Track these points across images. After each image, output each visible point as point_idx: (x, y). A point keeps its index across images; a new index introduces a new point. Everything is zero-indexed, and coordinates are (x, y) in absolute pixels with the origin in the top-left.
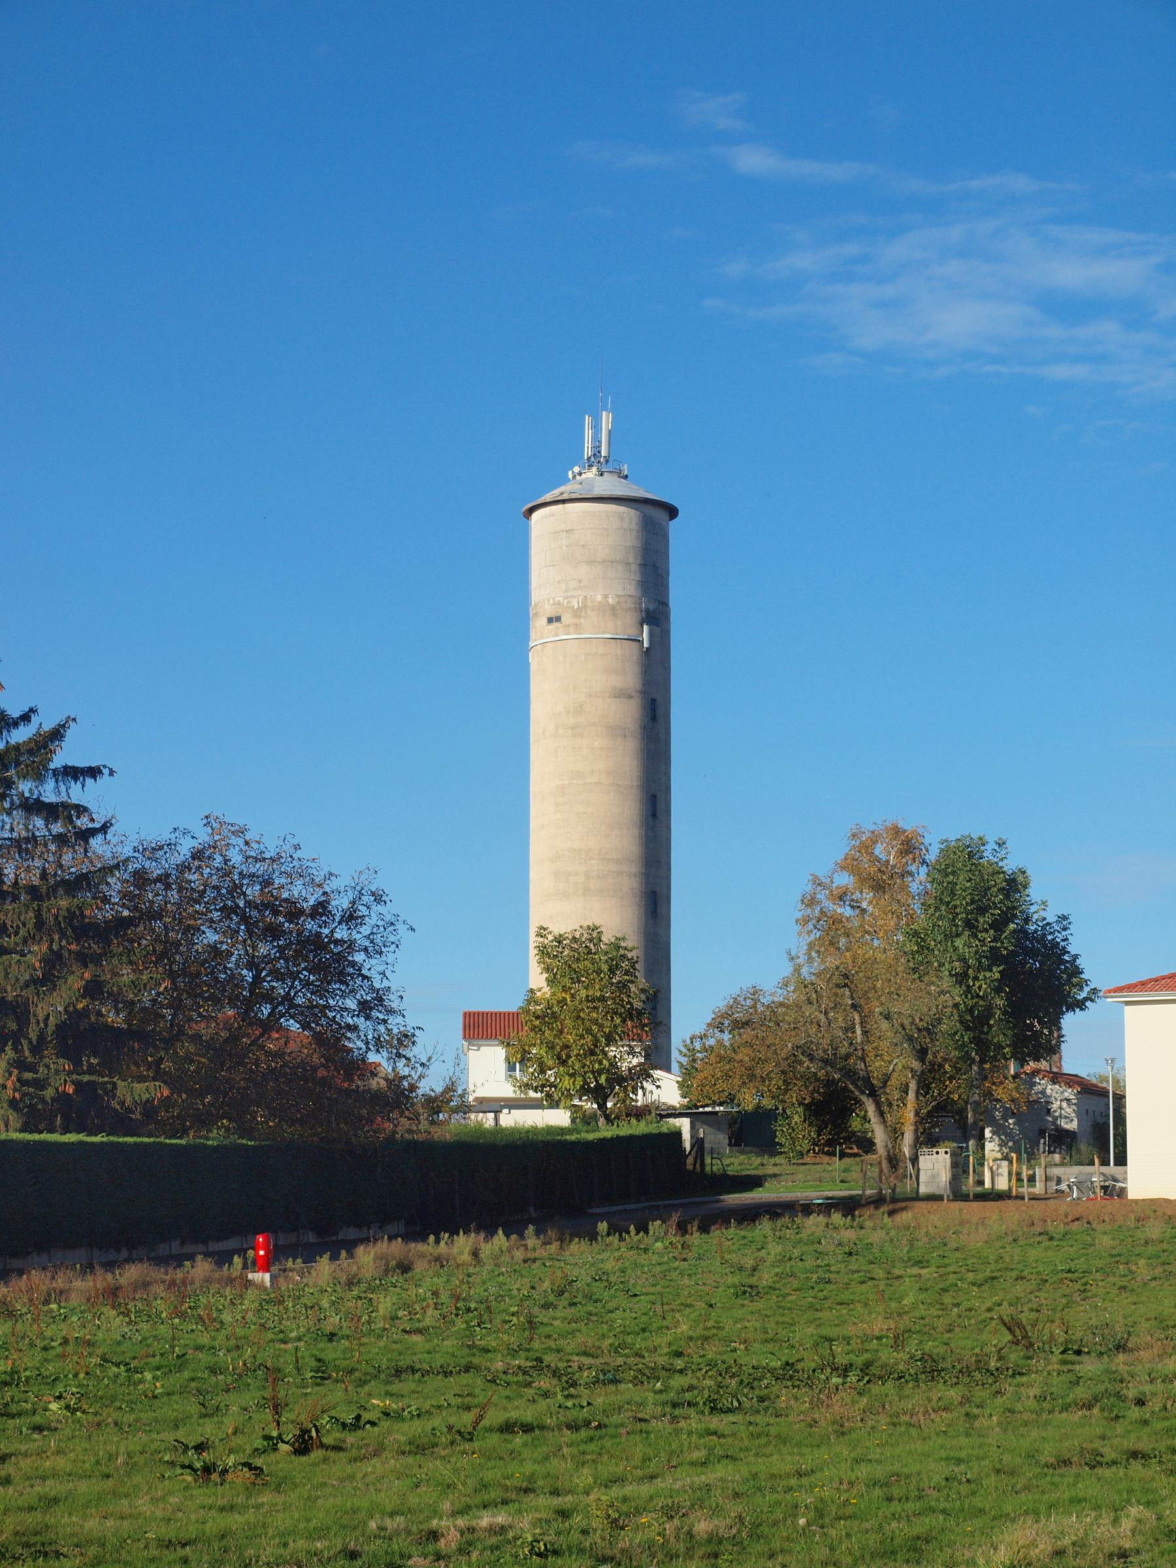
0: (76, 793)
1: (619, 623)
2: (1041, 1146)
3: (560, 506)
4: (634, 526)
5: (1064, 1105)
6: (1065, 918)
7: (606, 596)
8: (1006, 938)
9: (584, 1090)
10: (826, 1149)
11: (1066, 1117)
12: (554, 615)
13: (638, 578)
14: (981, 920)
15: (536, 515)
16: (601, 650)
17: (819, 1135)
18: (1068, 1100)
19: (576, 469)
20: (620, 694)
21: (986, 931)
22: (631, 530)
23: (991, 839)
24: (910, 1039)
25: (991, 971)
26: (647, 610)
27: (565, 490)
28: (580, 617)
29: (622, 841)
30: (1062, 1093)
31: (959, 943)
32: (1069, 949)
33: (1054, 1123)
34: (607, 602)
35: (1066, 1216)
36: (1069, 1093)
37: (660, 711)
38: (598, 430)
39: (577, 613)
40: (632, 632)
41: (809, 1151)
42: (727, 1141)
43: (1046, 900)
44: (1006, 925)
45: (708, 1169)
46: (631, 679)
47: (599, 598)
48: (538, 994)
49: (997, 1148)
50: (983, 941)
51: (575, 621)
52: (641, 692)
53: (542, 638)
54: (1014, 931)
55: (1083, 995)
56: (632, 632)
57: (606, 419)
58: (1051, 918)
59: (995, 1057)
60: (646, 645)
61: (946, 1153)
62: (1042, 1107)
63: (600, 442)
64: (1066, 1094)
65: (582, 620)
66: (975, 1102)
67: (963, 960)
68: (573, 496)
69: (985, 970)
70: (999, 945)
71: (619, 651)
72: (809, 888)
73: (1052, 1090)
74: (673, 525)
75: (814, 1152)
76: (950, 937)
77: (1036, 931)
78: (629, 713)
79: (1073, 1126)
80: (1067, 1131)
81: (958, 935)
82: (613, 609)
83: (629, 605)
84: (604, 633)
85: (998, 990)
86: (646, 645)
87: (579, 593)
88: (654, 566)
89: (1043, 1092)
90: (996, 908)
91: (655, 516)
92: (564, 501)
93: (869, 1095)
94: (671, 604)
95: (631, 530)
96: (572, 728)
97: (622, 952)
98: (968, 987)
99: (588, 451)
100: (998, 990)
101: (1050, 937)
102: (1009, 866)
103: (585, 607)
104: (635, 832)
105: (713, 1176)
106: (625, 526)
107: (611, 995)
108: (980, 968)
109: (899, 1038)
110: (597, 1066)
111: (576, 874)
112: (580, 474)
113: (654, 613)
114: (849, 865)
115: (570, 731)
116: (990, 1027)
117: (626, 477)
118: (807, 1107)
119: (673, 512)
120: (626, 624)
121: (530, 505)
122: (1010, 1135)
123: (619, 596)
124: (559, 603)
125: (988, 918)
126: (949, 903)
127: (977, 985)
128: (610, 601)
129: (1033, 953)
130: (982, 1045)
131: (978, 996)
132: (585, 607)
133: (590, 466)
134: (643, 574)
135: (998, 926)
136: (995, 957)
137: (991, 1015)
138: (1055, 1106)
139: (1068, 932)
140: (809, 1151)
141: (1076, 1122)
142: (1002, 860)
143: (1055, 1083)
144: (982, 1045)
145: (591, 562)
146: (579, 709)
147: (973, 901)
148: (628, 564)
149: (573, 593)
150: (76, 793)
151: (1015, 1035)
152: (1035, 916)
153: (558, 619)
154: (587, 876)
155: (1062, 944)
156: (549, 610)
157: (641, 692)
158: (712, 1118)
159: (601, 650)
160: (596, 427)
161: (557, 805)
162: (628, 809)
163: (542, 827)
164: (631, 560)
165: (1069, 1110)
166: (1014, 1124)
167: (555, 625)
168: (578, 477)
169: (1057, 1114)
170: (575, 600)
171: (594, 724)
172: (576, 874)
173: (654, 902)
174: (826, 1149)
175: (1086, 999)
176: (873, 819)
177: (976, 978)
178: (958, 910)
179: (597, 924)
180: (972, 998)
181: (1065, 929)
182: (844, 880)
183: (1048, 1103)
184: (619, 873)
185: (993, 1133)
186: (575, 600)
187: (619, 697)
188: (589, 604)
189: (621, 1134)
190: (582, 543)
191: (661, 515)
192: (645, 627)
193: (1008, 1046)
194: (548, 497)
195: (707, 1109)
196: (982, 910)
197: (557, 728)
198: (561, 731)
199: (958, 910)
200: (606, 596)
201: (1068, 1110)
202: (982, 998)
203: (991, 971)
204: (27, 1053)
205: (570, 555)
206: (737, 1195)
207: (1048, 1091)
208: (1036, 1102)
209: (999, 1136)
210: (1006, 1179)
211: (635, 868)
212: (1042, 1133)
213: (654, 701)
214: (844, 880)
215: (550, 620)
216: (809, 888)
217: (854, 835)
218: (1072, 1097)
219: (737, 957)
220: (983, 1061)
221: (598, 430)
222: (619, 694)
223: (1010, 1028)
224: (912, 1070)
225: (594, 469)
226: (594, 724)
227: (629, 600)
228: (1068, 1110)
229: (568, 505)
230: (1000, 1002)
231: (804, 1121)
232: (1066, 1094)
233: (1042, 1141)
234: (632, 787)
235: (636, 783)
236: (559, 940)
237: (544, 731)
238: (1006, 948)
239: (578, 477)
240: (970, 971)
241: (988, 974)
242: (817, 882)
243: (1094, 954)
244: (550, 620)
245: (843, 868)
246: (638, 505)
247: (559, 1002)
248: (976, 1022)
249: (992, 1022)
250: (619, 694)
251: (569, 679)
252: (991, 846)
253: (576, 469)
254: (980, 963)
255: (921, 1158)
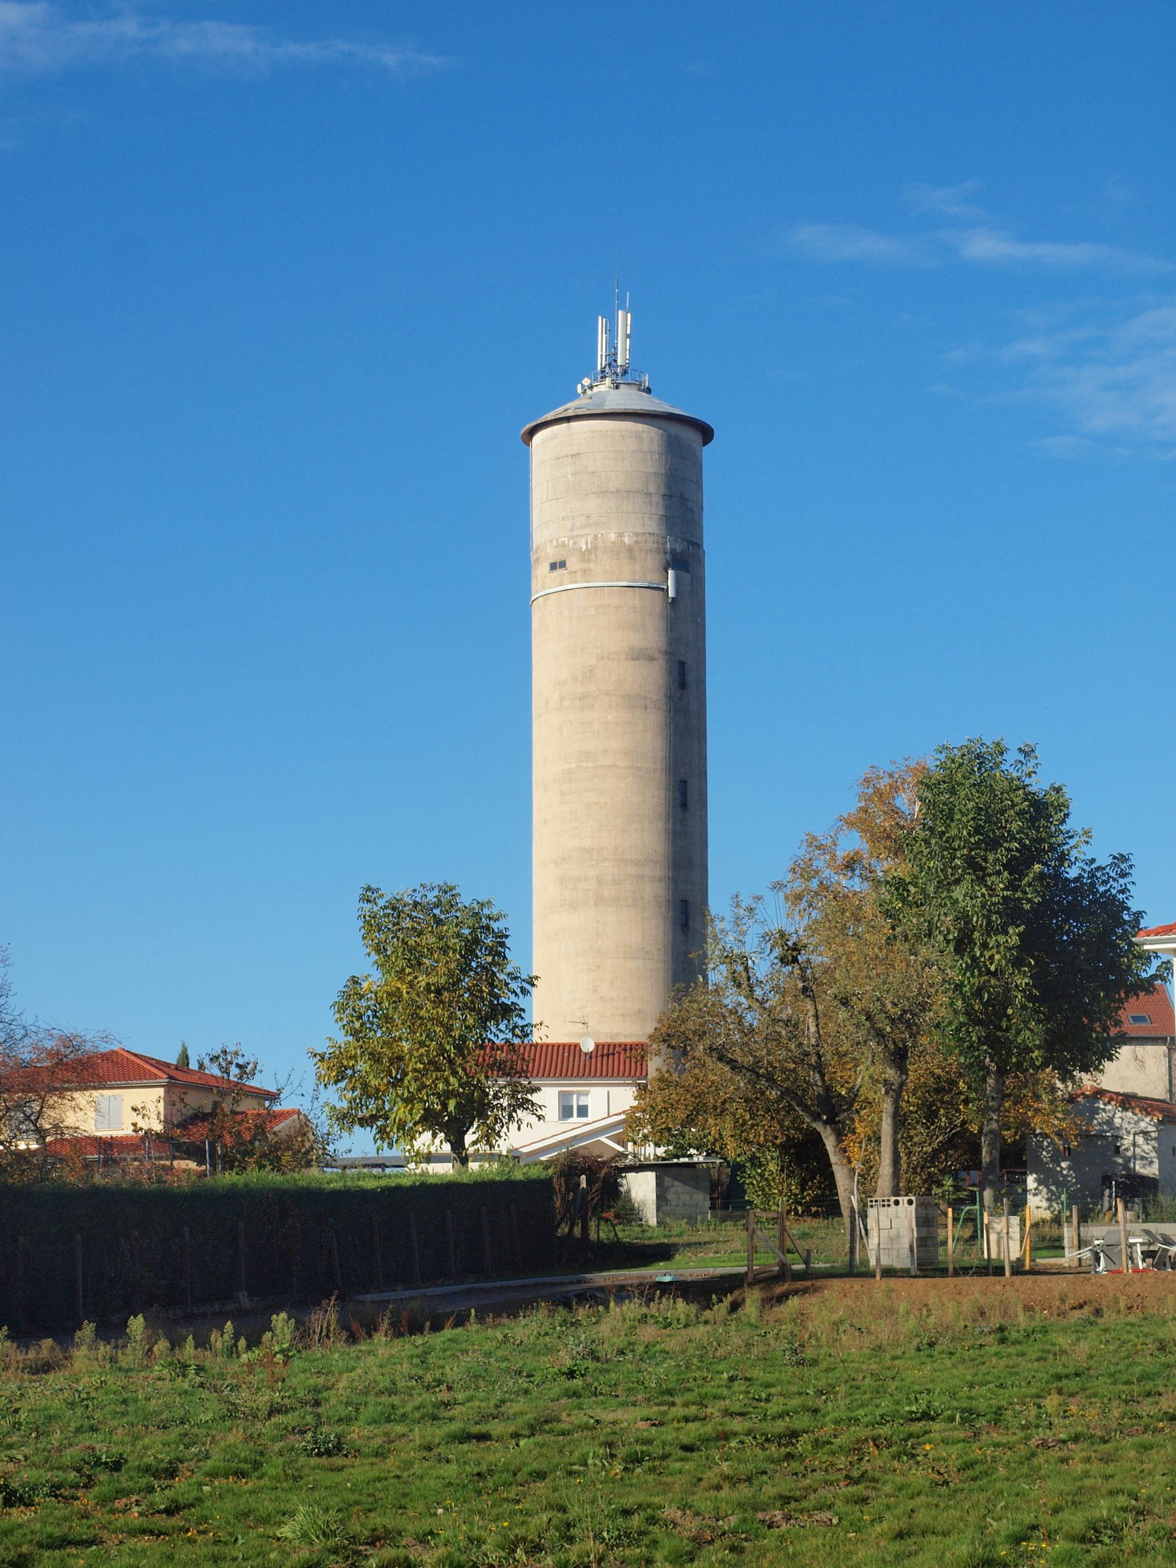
1: (638, 567)
2: (1106, 1199)
3: (565, 426)
4: (655, 447)
5: (1140, 1140)
6: (1123, 858)
7: (621, 535)
8: (1030, 885)
9: (430, 1120)
10: (814, 1209)
11: (1143, 1158)
12: (558, 559)
13: (661, 512)
14: (991, 857)
15: (538, 438)
16: (615, 601)
17: (803, 1190)
18: (1145, 1133)
19: (586, 382)
21: (999, 873)
22: (651, 452)
23: (1013, 744)
24: (880, 1035)
25: (1006, 933)
26: (673, 552)
27: (571, 408)
28: (589, 561)
29: (643, 837)
30: (1136, 1123)
31: (958, 893)
32: (1129, 903)
33: (1125, 1166)
34: (622, 542)
35: (1063, 1301)
36: (1147, 1123)
37: (691, 677)
38: (616, 335)
39: (585, 556)
40: (654, 578)
41: (788, 1212)
42: (708, 1203)
43: (1094, 835)
44: (1029, 866)
45: (593, 1236)
46: (653, 637)
47: (613, 537)
48: (365, 985)
49: (1045, 1204)
50: (991, 889)
51: (583, 566)
52: (666, 653)
53: (544, 588)
54: (1041, 876)
55: (1152, 971)
56: (654, 578)
57: (624, 321)
58: (1103, 860)
59: (1019, 1065)
60: (671, 594)
61: (910, 1202)
62: (1106, 1145)
63: (616, 348)
64: (1143, 1125)
65: (592, 565)
66: (992, 1132)
67: (964, 917)
68: (579, 412)
69: (997, 933)
70: (1019, 894)
71: (637, 603)
72: (802, 852)
73: (1122, 1118)
74: (709, 453)
75: (796, 1213)
76: (947, 884)
77: (1078, 879)
78: (650, 679)
79: (1152, 1171)
80: (1143, 1178)
81: (957, 882)
82: (630, 550)
83: (650, 545)
84: (618, 580)
85: (1017, 963)
86: (671, 594)
87: (584, 532)
88: (682, 497)
89: (1110, 1122)
90: (1013, 838)
91: (683, 440)
92: (568, 419)
93: (826, 1123)
94: (706, 546)
95: (651, 452)
96: (580, 699)
97: (484, 922)
98: (974, 958)
99: (601, 361)
100: (1017, 963)
101: (1102, 889)
102: (1039, 785)
103: (596, 548)
104: (661, 825)
105: (600, 1244)
106: (645, 447)
108: (990, 930)
109: (861, 1035)
110: (441, 1086)
111: (586, 879)
112: (591, 387)
113: (683, 554)
114: (861, 822)
115: (578, 702)
116: (1009, 1018)
117: (648, 391)
118: (784, 1148)
119: (706, 433)
120: (647, 568)
121: (529, 426)
122: (1061, 1184)
123: (637, 535)
124: (564, 545)
125: (1001, 855)
126: (943, 833)
127: (987, 954)
128: (627, 540)
129: (1072, 911)
130: (997, 1043)
131: (988, 972)
132: (596, 548)
133: (603, 377)
134: (667, 507)
135: (1016, 867)
136: (1012, 912)
137: (1008, 1001)
138: (1127, 1141)
139: (1128, 879)
140: (788, 1212)
141: (1156, 1166)
142: (1029, 775)
143: (1125, 1109)
144: (997, 1043)
145: (603, 493)
147: (977, 830)
148: (648, 494)
149: (579, 532)
151: (1048, 1031)
152: (1074, 853)
153: (563, 564)
154: (600, 882)
155: (1120, 896)
157: (666, 653)
158: (687, 1171)
159: (615, 601)
160: (611, 331)
161: (563, 794)
163: (546, 822)
164: (652, 489)
165: (1146, 1147)
166: (1069, 1168)
167: (559, 572)
168: (589, 392)
169: (1130, 1154)
170: (583, 541)
171: (607, 693)
172: (586, 879)
174: (814, 1209)
175: (1154, 977)
177: (985, 946)
178: (956, 844)
179: (451, 883)
180: (980, 975)
181: (1124, 875)
182: (852, 842)
183: (1117, 1137)
184: (640, 877)
185: (1039, 1182)
186: (583, 541)
187: (637, 659)
188: (600, 544)
190: (591, 469)
191: (693, 437)
192: (671, 572)
193: (1038, 1047)
194: (550, 416)
195: (682, 1160)
196: (993, 844)
197: (562, 699)
198: (567, 703)
199: (956, 844)
200: (621, 535)
201: (1146, 1148)
202: (994, 974)
203: (1006, 933)
204: (950, 1214)
205: (579, 487)
206: (626, 1272)
207: (1117, 1121)
208: (1100, 1136)
209: (1047, 1186)
210: (1018, 1243)
211: (659, 871)
212: (1106, 1180)
213: (682, 664)
214: (852, 842)
215: (553, 567)
216: (802, 852)
217: (867, 781)
218: (1151, 1128)
220: (1002, 1072)
221: (616, 335)
222: (637, 655)
223: (1039, 1022)
224: (886, 1082)
225: (608, 381)
226: (607, 693)
227: (650, 539)
228: (1146, 1148)
229: (575, 425)
230: (1022, 981)
231: (782, 1170)
232: (1143, 1125)
233: (1107, 1192)
234: (655, 770)
235: (659, 765)
236: (394, 907)
237: (547, 703)
238: (1029, 901)
239: (589, 392)
240: (976, 935)
241: (1002, 939)
242: (813, 843)
244: (553, 567)
245: (850, 824)
246: (663, 423)
247: (390, 994)
248: (987, 1016)
249: (1010, 1011)
250: (637, 655)
251: (580, 635)
252: (1012, 756)
253: (586, 382)
254: (989, 922)
255: (872, 1213)
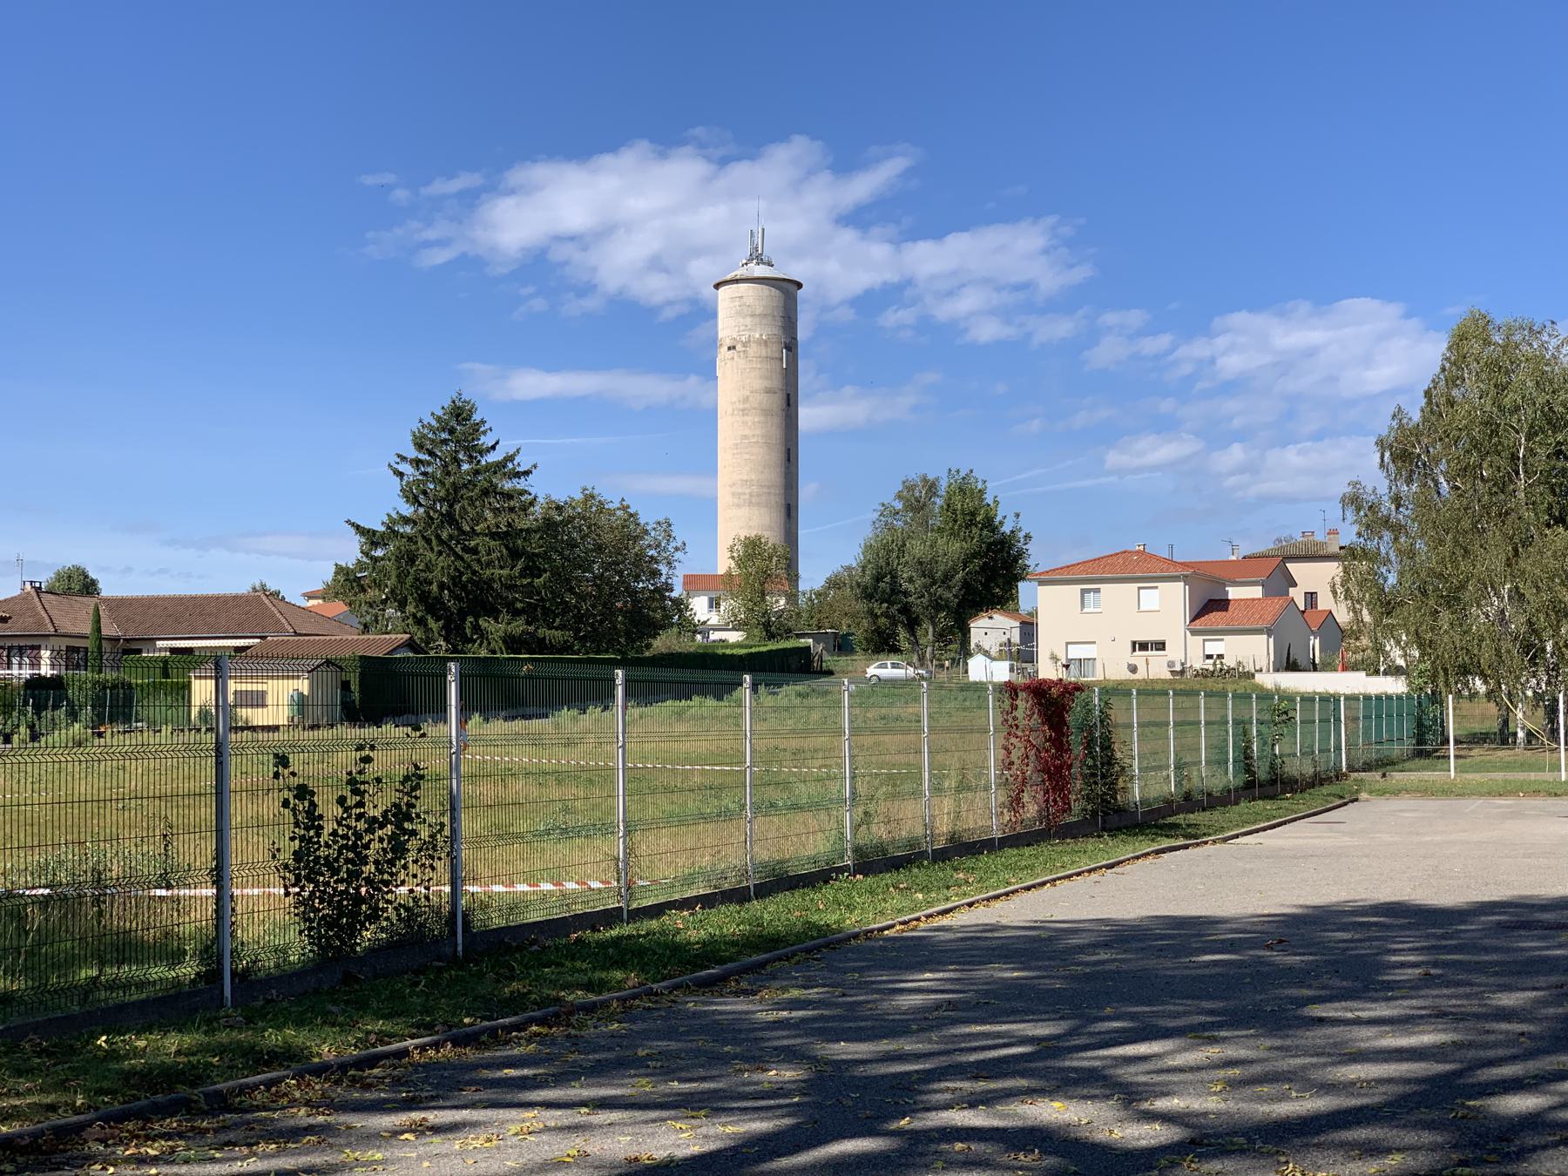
0: (521, 484)
15: (722, 289)
20: (766, 412)
39: (745, 344)
46: (776, 382)
78: (777, 401)
107: (768, 564)
114: (899, 497)
119: (799, 285)
120: (773, 351)
145: (753, 315)
146: (746, 399)
150: (521, 484)
156: (728, 342)
162: (777, 456)
173: (790, 511)
176: (914, 475)
189: (677, 649)
214: (899, 505)
219: (830, 554)
222: (768, 391)
243: (1037, 557)
250: (768, 391)
